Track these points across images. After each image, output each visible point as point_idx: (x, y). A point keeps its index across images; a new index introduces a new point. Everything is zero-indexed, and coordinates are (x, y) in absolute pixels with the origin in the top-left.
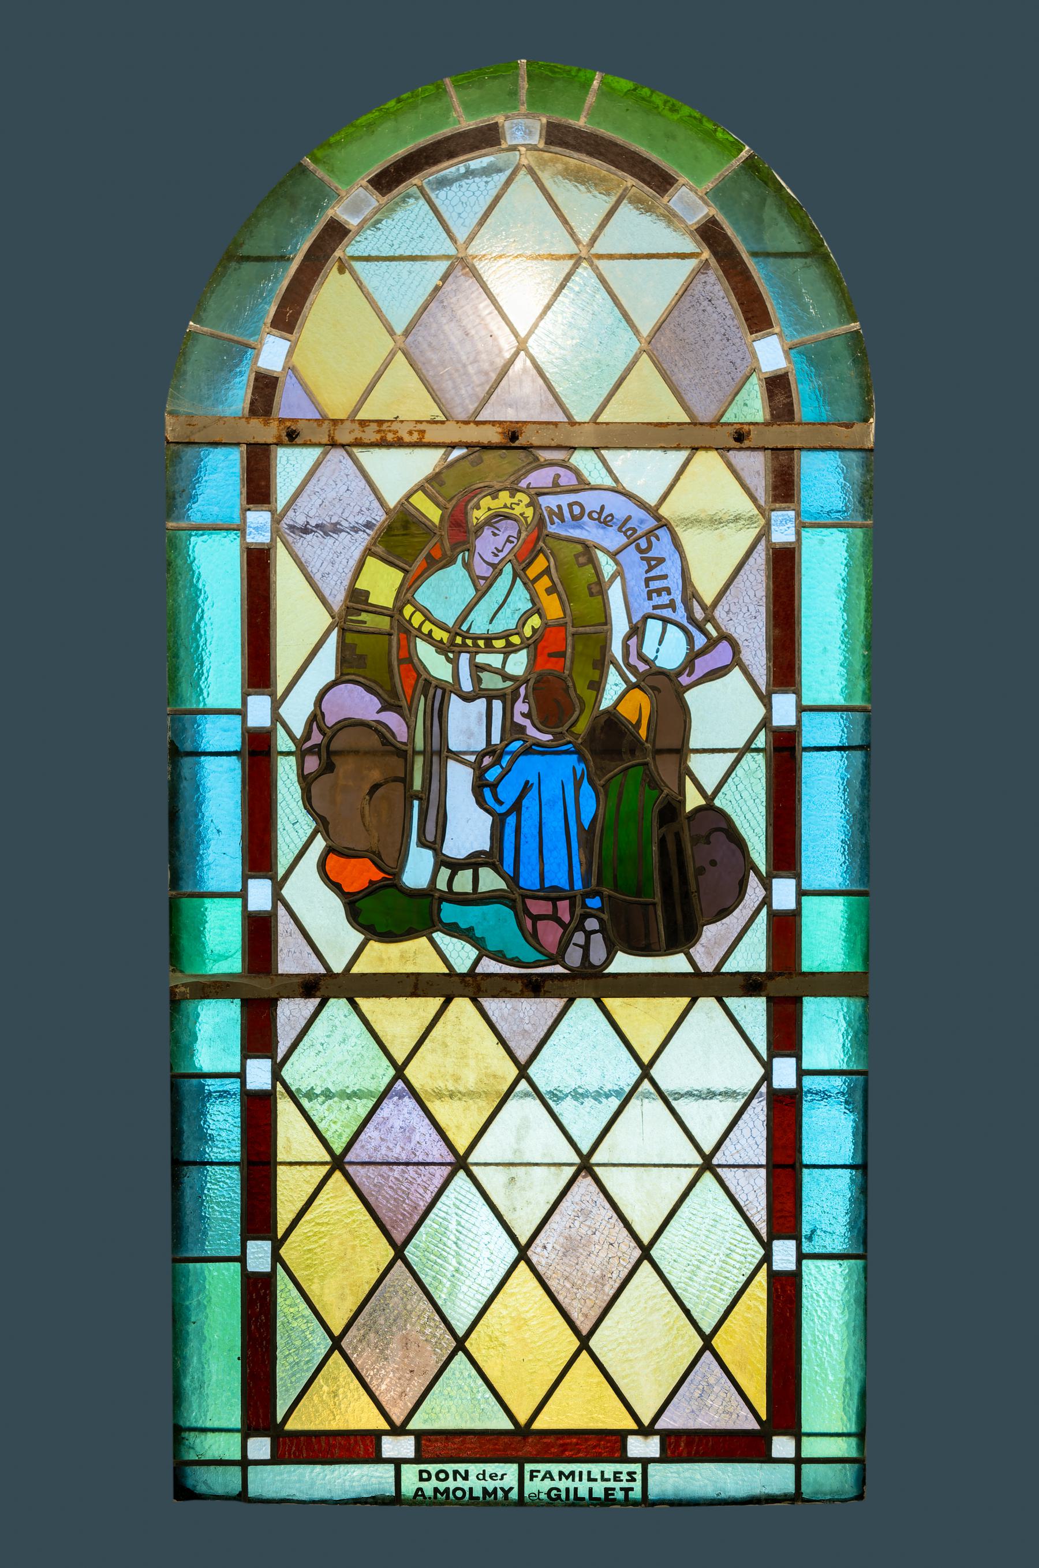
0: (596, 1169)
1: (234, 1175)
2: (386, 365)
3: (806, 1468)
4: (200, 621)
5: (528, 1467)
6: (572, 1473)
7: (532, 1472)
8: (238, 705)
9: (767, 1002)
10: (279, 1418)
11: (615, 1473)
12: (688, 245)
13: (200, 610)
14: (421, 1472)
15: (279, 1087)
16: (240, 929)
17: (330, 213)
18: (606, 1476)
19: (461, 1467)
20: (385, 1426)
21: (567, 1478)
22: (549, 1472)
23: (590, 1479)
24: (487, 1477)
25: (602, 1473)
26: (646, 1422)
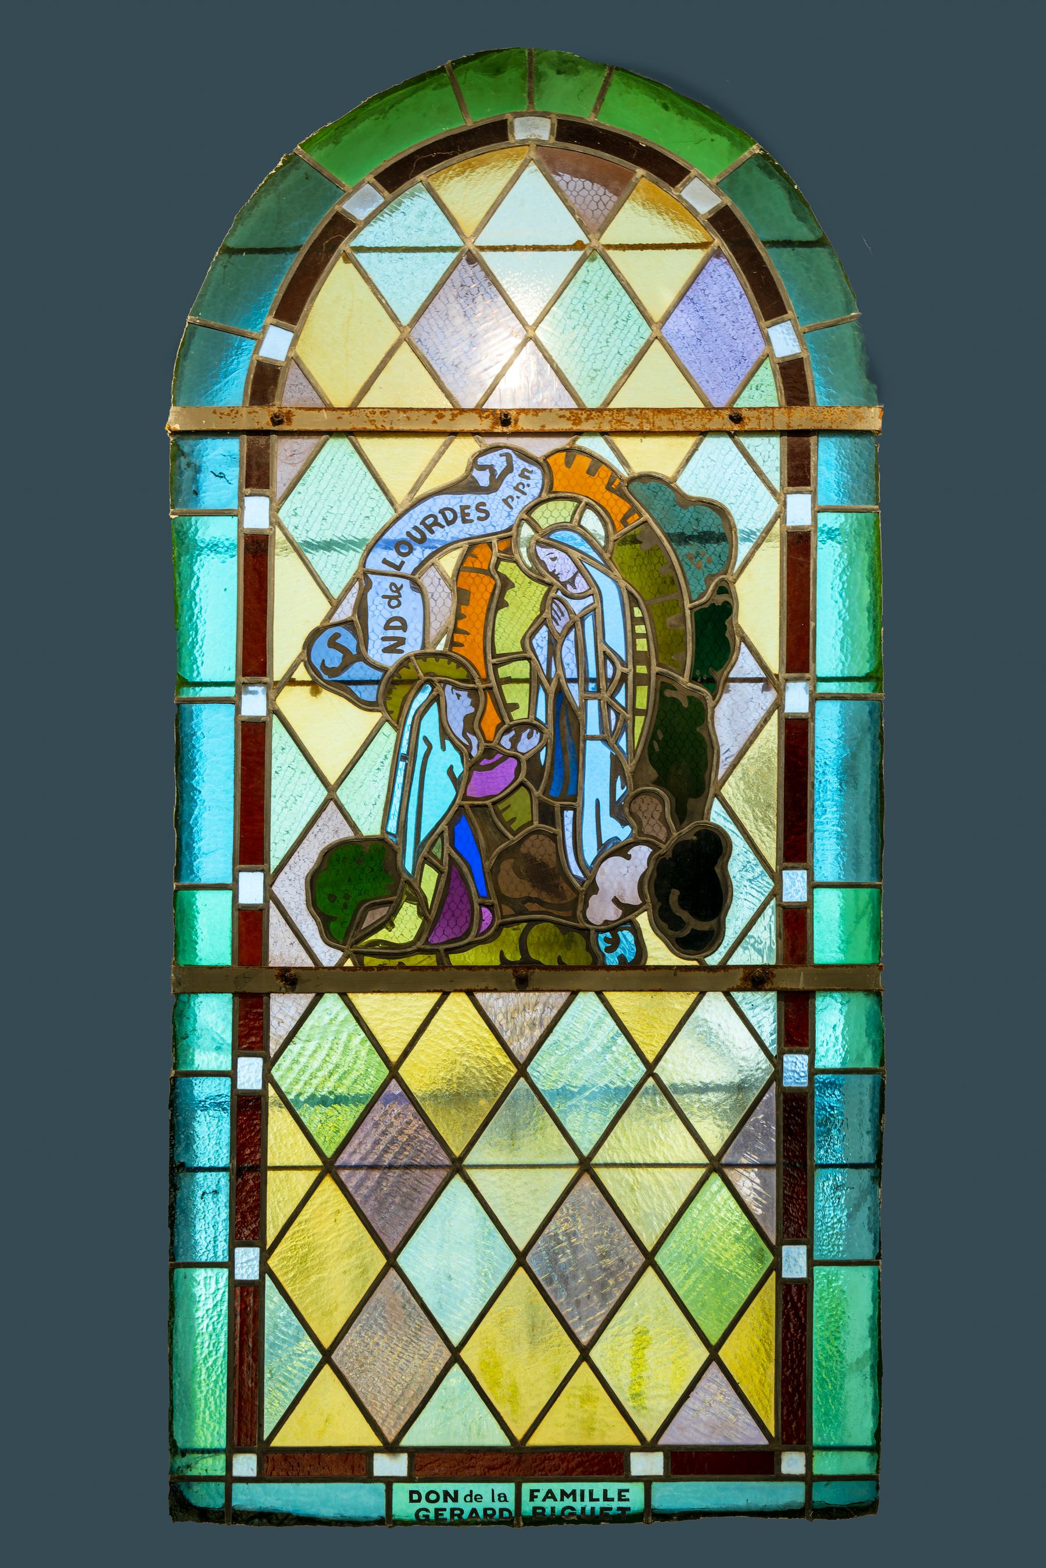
0: (597, 1170)
1: (223, 1180)
2: (390, 354)
3: (237, 1487)
4: (195, 588)
5: (526, 1487)
6: (574, 1492)
7: (532, 1491)
8: (229, 880)
9: (779, 999)
10: (266, 1436)
11: (620, 1491)
12: (701, 237)
13: (195, 578)
14: (412, 1493)
15: (271, 1092)
16: (230, 934)
17: (337, 208)
18: (609, 1496)
19: (451, 1487)
20: (375, 1441)
21: (568, 1497)
22: (550, 1491)
23: (592, 1499)
24: (496, 1498)
25: (605, 1492)
26: (649, 1436)
